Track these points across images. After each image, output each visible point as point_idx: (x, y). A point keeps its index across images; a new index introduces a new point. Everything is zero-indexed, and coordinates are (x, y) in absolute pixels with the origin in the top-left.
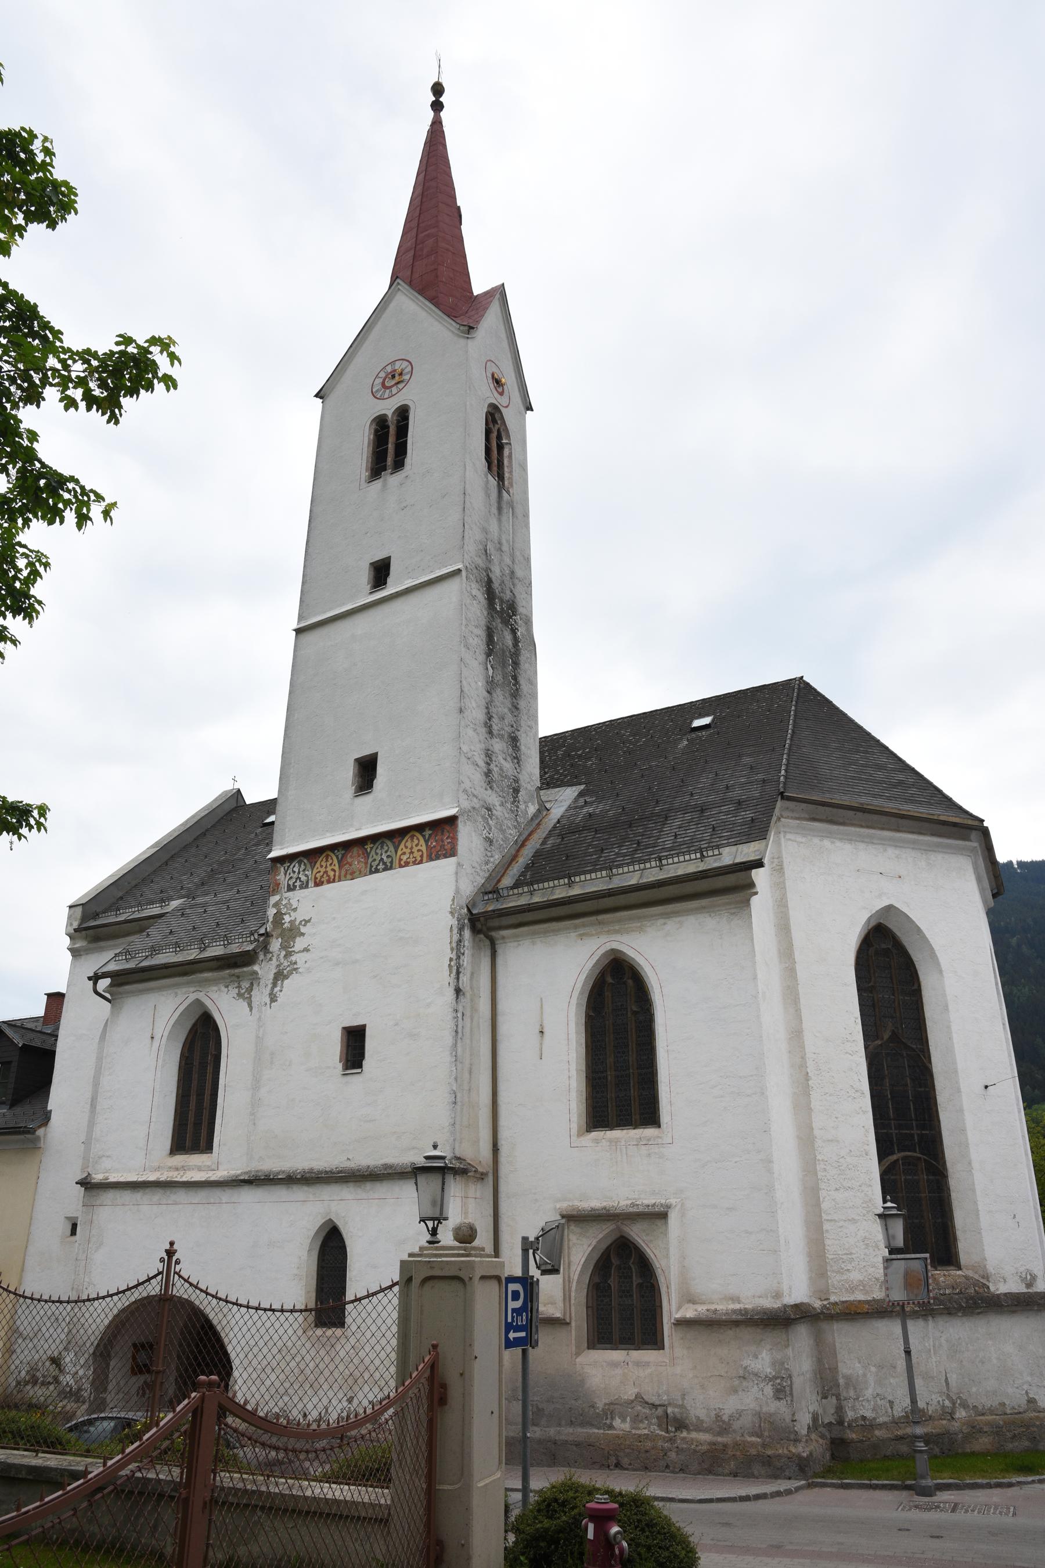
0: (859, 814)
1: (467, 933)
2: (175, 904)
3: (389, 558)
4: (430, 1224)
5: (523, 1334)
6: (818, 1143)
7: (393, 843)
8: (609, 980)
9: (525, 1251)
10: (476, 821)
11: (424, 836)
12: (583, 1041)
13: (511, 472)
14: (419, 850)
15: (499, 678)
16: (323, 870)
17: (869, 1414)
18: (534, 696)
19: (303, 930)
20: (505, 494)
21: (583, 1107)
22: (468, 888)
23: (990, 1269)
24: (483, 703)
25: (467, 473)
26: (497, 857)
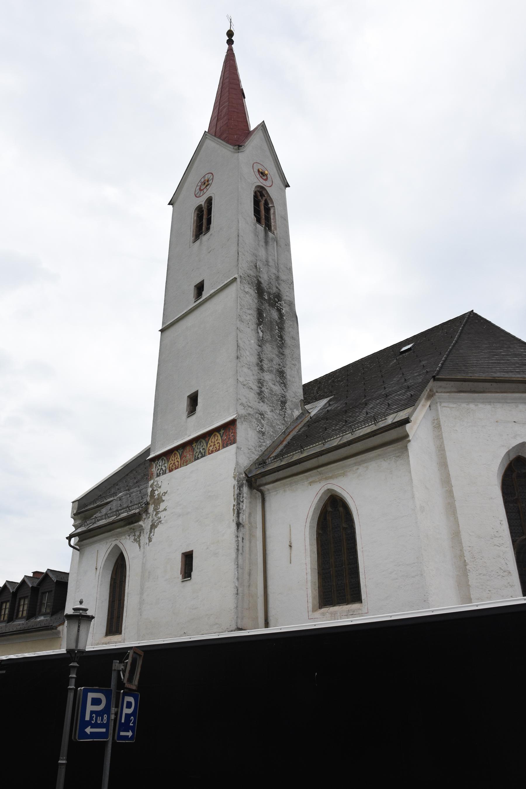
0: (494, 384)
1: (245, 489)
7: (205, 441)
8: (329, 509)
10: (251, 422)
11: (220, 434)
12: (315, 550)
13: (275, 222)
14: (218, 443)
15: (268, 337)
18: (297, 346)
19: (164, 498)
20: (270, 234)
21: (316, 593)
22: (245, 462)
24: (256, 352)
25: (240, 225)
26: (268, 442)
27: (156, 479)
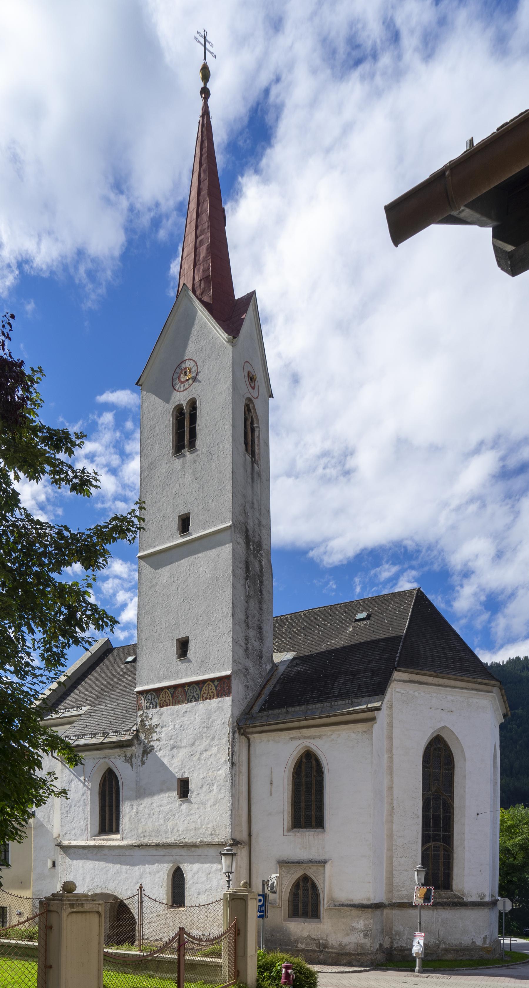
1: (237, 735)
2: (85, 709)
3: (189, 513)
4: (227, 874)
5: (263, 914)
6: (395, 837)
8: (304, 760)
9: (263, 885)
13: (259, 449)
14: (212, 692)
15: (252, 593)
16: (164, 699)
17: (404, 945)
20: (256, 466)
23: (466, 892)
26: (251, 695)
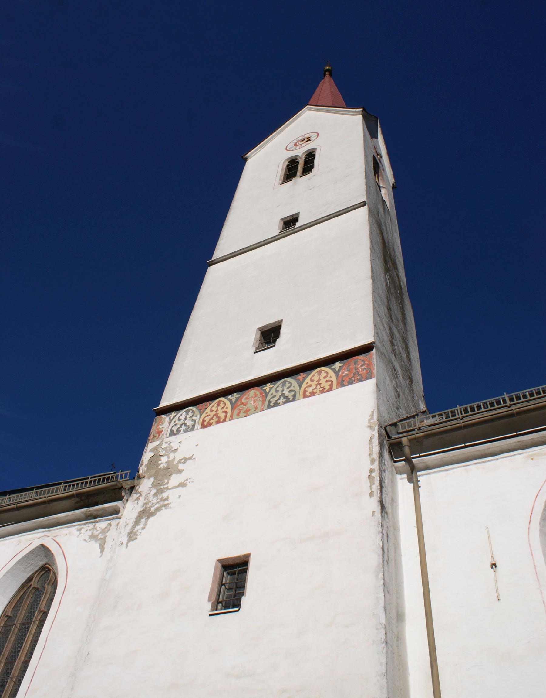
11: (334, 370)
27: (166, 440)
